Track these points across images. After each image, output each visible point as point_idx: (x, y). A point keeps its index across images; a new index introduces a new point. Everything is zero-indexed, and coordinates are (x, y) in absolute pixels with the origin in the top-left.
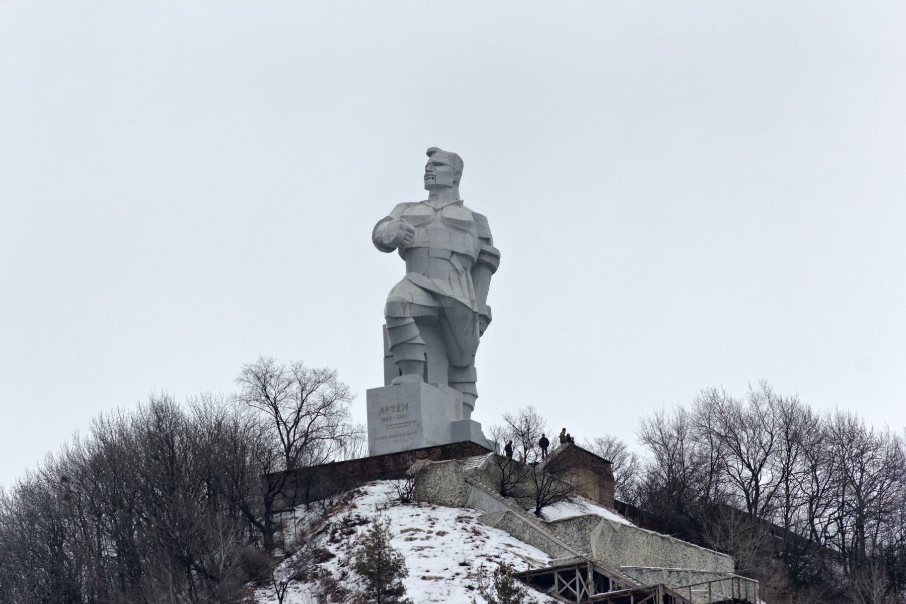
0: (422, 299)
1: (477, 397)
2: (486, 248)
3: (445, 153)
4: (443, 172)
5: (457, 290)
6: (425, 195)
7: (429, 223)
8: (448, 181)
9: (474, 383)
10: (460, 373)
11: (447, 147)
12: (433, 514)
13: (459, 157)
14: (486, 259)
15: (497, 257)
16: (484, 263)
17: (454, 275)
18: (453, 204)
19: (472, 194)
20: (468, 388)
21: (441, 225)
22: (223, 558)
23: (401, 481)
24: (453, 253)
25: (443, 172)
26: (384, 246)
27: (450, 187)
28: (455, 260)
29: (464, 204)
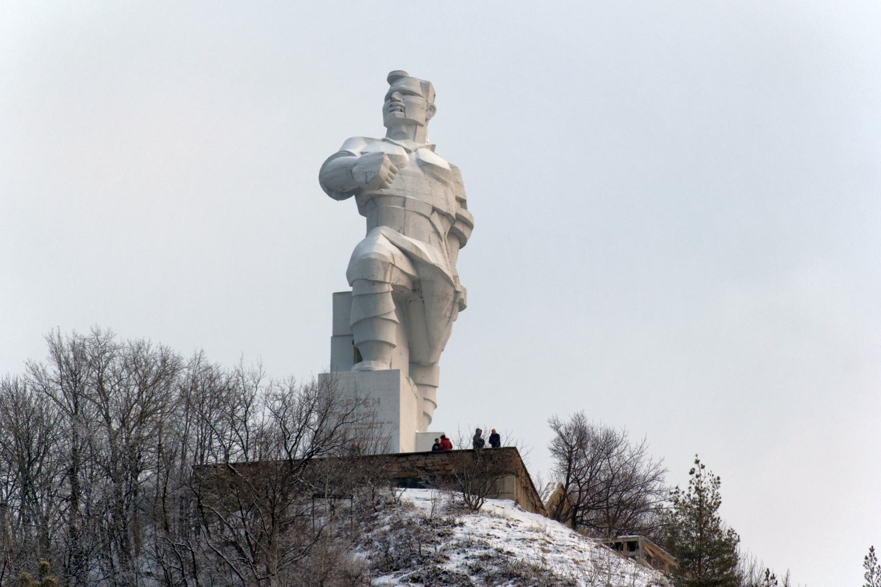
0: (403, 264)
2: (463, 212)
4: (403, 106)
11: (416, 72)
14: (459, 226)
16: (458, 230)
17: (434, 237)
19: (442, 140)
24: (434, 209)
25: (403, 106)
28: (435, 218)
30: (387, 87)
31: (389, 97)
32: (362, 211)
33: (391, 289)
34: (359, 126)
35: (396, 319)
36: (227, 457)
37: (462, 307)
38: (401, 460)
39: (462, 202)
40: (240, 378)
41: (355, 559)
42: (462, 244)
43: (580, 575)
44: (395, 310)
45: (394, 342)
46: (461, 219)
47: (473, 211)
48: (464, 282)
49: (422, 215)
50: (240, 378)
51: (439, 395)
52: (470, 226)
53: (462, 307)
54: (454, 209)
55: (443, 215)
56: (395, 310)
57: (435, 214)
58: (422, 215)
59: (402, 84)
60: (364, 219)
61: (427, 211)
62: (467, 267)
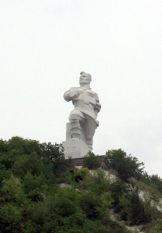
0: (82, 116)
1: (92, 149)
2: (98, 104)
3: (86, 73)
4: (85, 80)
5: (90, 113)
6: (79, 86)
7: (83, 93)
8: (87, 82)
9: (92, 144)
10: (88, 140)
11: (87, 72)
12: (80, 183)
13: (91, 76)
14: (97, 107)
15: (100, 107)
16: (97, 108)
17: (90, 109)
18: (89, 89)
19: (94, 87)
20: (90, 146)
21: (86, 94)
22: (71, 152)
23: (161, 220)
24: (90, 103)
25: (85, 80)
26: (68, 98)
27: (88, 84)
28: (90, 105)
29: (92, 89)
32: (74, 104)
33: (79, 121)
35: (80, 128)
38: (78, 159)
39: (98, 101)
41: (98, 176)
42: (99, 111)
43: (2, 225)
44: (84, 126)
45: (80, 134)
46: (97, 105)
47: (101, 103)
49: (87, 104)
51: (93, 146)
53: (98, 125)
54: (94, 102)
55: (92, 104)
56: (84, 126)
57: (90, 104)
58: (87, 104)
60: (74, 106)
61: (88, 103)
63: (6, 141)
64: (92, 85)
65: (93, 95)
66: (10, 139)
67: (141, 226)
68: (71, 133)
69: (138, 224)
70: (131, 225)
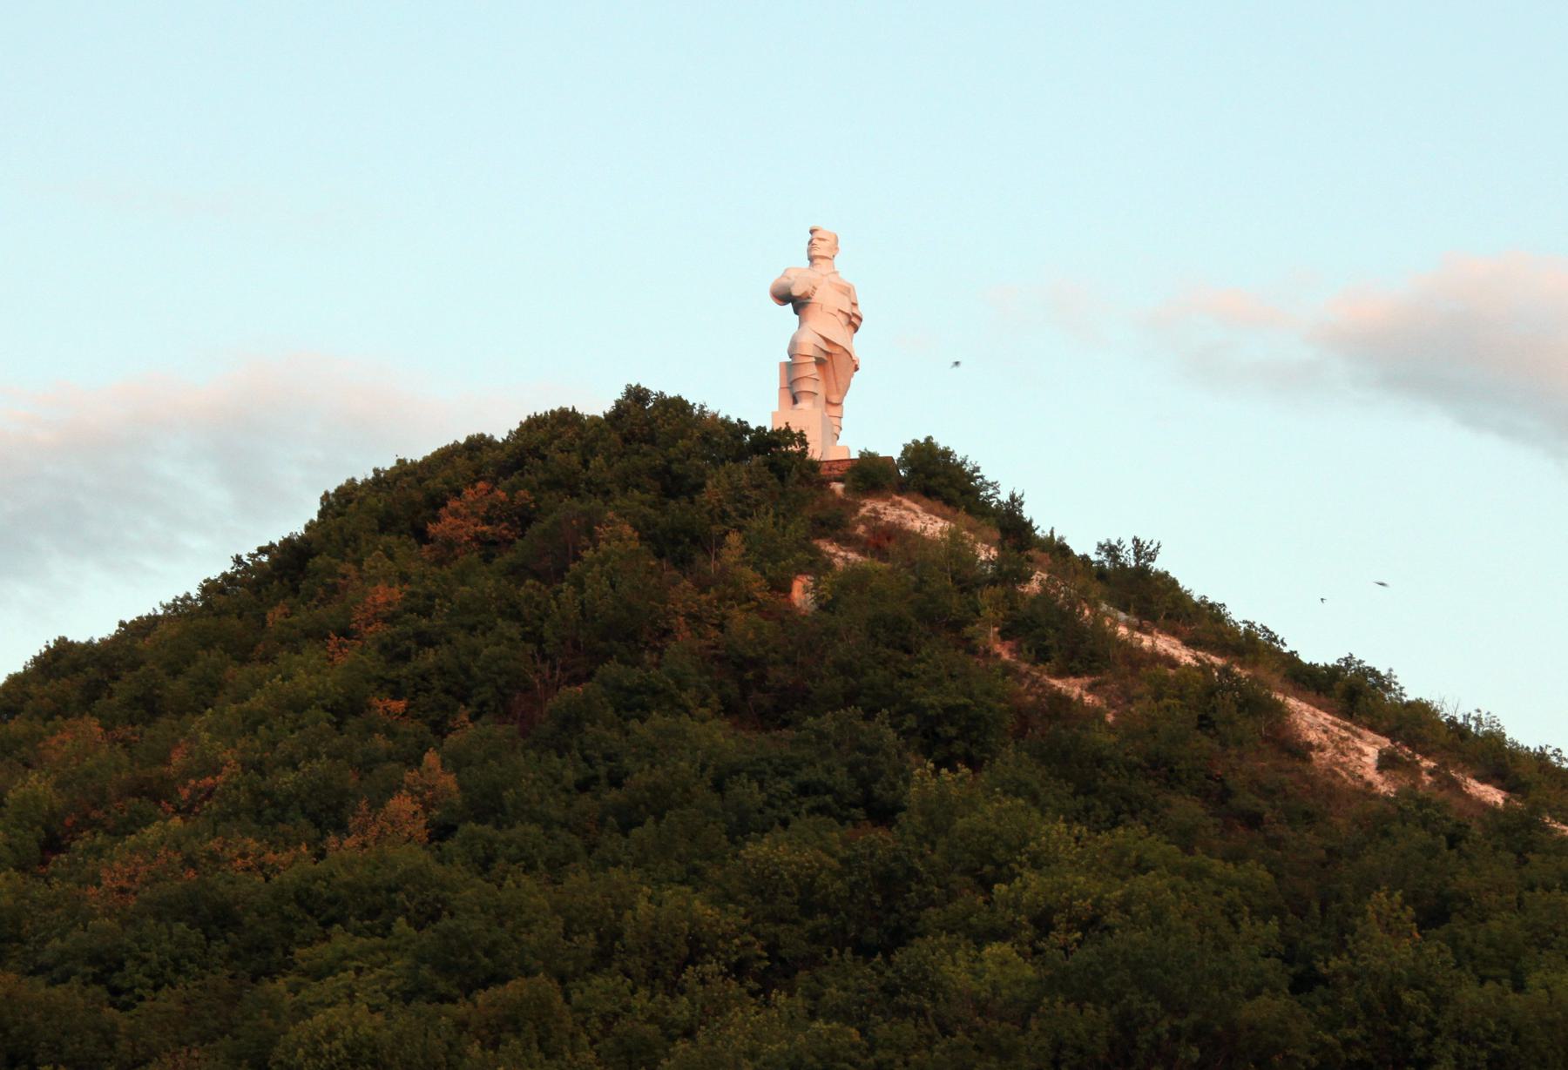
4: (819, 249)
5: (838, 334)
11: (827, 226)
14: (854, 320)
16: (854, 322)
19: (846, 267)
25: (819, 249)
26: (783, 296)
30: (809, 237)
31: (810, 242)
32: (796, 312)
34: (790, 262)
36: (355, 1030)
37: (856, 369)
39: (855, 304)
40: (1249, 893)
44: (822, 369)
47: (861, 309)
48: (856, 354)
50: (1249, 893)
52: (860, 319)
53: (856, 369)
59: (817, 234)
62: (859, 345)
63: (224, 575)
64: (839, 262)
65: (847, 291)
66: (188, 596)
67: (1087, 680)
68: (793, 393)
69: (1076, 675)
70: (1060, 674)
